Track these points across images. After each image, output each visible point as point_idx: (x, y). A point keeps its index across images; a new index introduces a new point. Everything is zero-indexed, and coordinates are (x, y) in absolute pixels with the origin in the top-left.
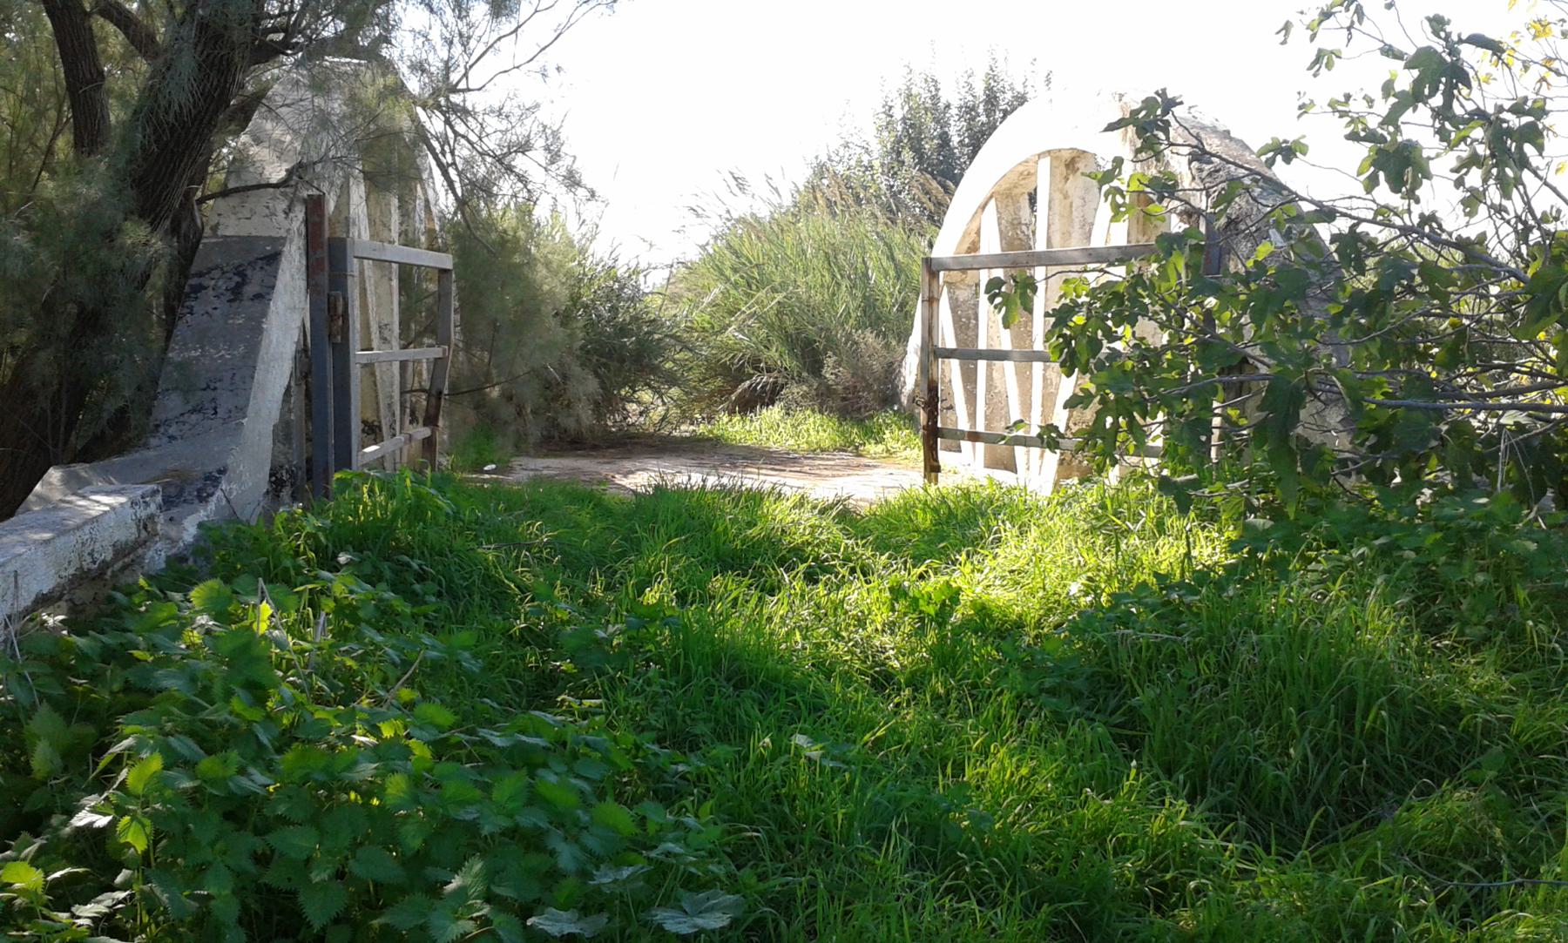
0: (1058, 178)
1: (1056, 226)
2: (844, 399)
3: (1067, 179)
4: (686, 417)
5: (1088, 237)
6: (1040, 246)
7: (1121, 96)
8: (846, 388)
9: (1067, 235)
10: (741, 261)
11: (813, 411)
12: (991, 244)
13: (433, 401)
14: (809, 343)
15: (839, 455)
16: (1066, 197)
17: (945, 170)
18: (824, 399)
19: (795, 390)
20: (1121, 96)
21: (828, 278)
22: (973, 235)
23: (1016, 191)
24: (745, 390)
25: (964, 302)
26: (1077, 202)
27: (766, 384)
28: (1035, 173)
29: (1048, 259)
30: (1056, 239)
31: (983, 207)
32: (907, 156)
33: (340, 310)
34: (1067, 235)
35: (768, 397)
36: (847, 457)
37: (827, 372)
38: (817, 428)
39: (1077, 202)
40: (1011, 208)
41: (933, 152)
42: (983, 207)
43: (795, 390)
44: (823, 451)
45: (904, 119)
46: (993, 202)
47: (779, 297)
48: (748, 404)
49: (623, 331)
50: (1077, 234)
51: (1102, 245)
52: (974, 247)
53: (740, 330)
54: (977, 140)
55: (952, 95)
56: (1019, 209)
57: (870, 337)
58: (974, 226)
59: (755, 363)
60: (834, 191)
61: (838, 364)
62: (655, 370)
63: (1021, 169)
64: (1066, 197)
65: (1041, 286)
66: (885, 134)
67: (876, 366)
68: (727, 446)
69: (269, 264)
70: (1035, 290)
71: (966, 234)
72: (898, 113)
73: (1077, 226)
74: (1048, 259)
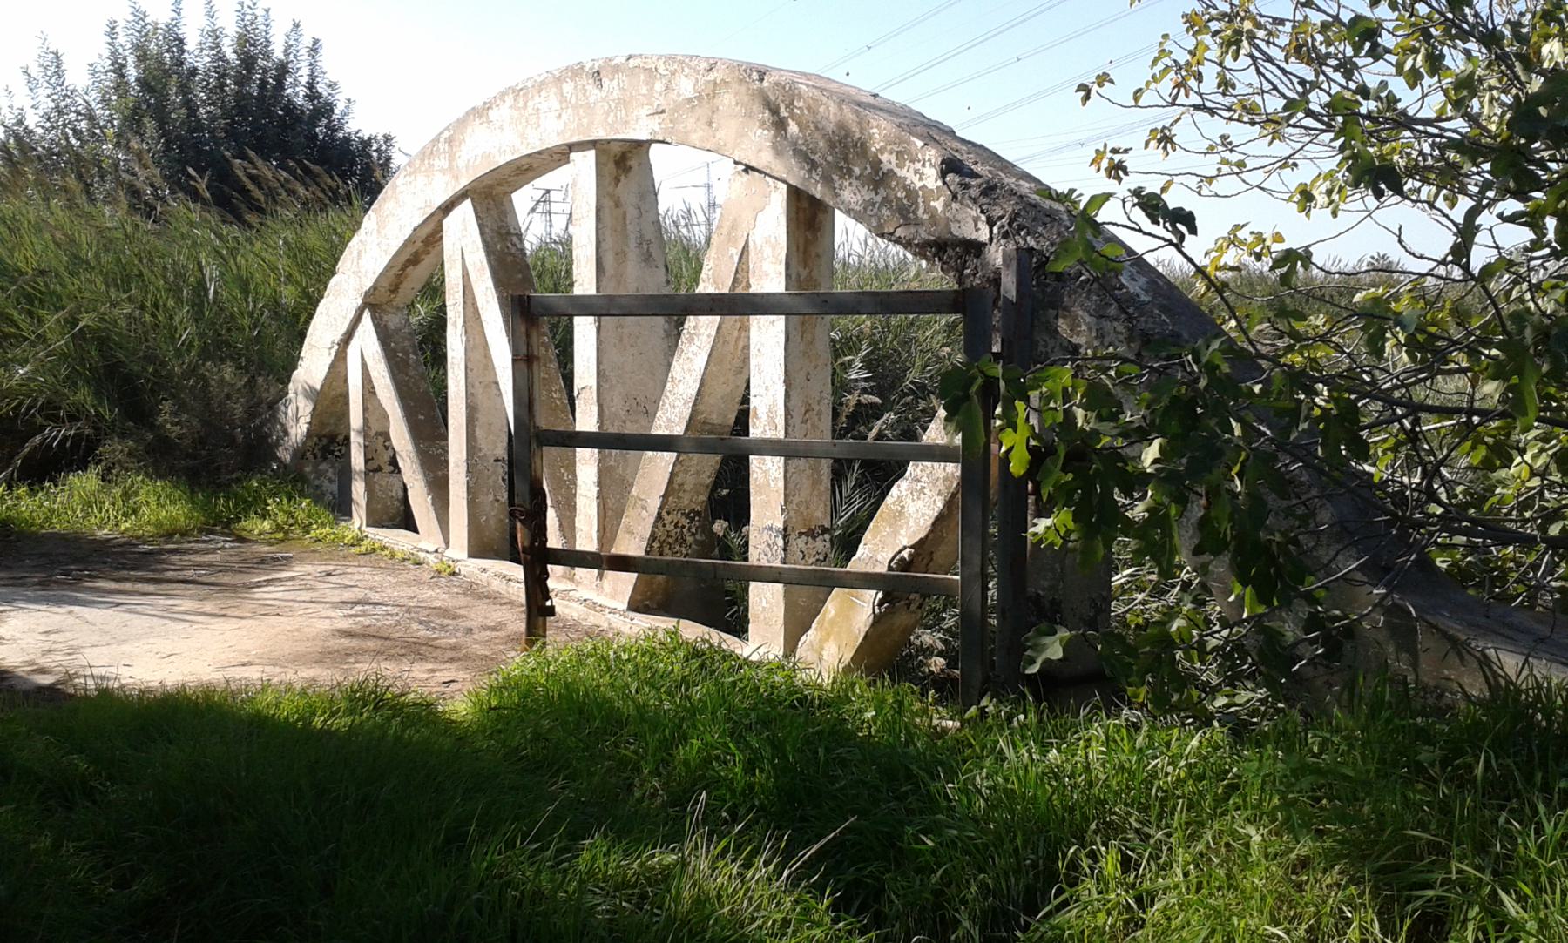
1: (608, 244)
3: (617, 181)
16: (617, 205)
18: (162, 459)
25: (398, 330)
26: (632, 212)
27: (65, 438)
31: (447, 208)
32: (150, 125)
35: (76, 456)
36: (220, 550)
38: (158, 506)
39: (632, 212)
43: (114, 448)
44: (184, 534)
45: (137, 80)
46: (467, 205)
48: (44, 470)
55: (197, 56)
59: (51, 412)
61: (182, 407)
62: (1493, 687)
64: (617, 205)
73: (632, 244)
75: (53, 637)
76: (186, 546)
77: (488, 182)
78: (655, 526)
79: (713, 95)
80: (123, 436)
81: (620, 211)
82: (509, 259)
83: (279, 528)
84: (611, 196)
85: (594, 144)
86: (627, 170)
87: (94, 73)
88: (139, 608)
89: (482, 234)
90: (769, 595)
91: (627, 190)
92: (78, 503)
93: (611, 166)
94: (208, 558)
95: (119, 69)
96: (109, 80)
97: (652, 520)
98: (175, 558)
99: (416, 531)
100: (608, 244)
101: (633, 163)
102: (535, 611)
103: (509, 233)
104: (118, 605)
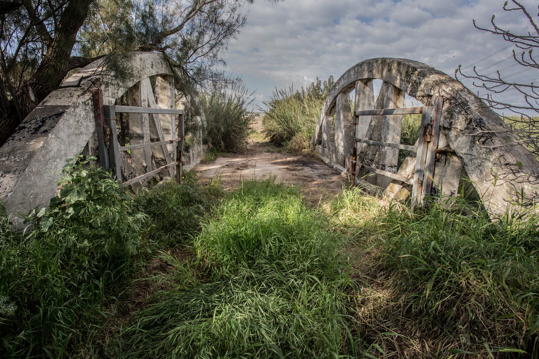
33: (108, 132)
88: (518, 44)
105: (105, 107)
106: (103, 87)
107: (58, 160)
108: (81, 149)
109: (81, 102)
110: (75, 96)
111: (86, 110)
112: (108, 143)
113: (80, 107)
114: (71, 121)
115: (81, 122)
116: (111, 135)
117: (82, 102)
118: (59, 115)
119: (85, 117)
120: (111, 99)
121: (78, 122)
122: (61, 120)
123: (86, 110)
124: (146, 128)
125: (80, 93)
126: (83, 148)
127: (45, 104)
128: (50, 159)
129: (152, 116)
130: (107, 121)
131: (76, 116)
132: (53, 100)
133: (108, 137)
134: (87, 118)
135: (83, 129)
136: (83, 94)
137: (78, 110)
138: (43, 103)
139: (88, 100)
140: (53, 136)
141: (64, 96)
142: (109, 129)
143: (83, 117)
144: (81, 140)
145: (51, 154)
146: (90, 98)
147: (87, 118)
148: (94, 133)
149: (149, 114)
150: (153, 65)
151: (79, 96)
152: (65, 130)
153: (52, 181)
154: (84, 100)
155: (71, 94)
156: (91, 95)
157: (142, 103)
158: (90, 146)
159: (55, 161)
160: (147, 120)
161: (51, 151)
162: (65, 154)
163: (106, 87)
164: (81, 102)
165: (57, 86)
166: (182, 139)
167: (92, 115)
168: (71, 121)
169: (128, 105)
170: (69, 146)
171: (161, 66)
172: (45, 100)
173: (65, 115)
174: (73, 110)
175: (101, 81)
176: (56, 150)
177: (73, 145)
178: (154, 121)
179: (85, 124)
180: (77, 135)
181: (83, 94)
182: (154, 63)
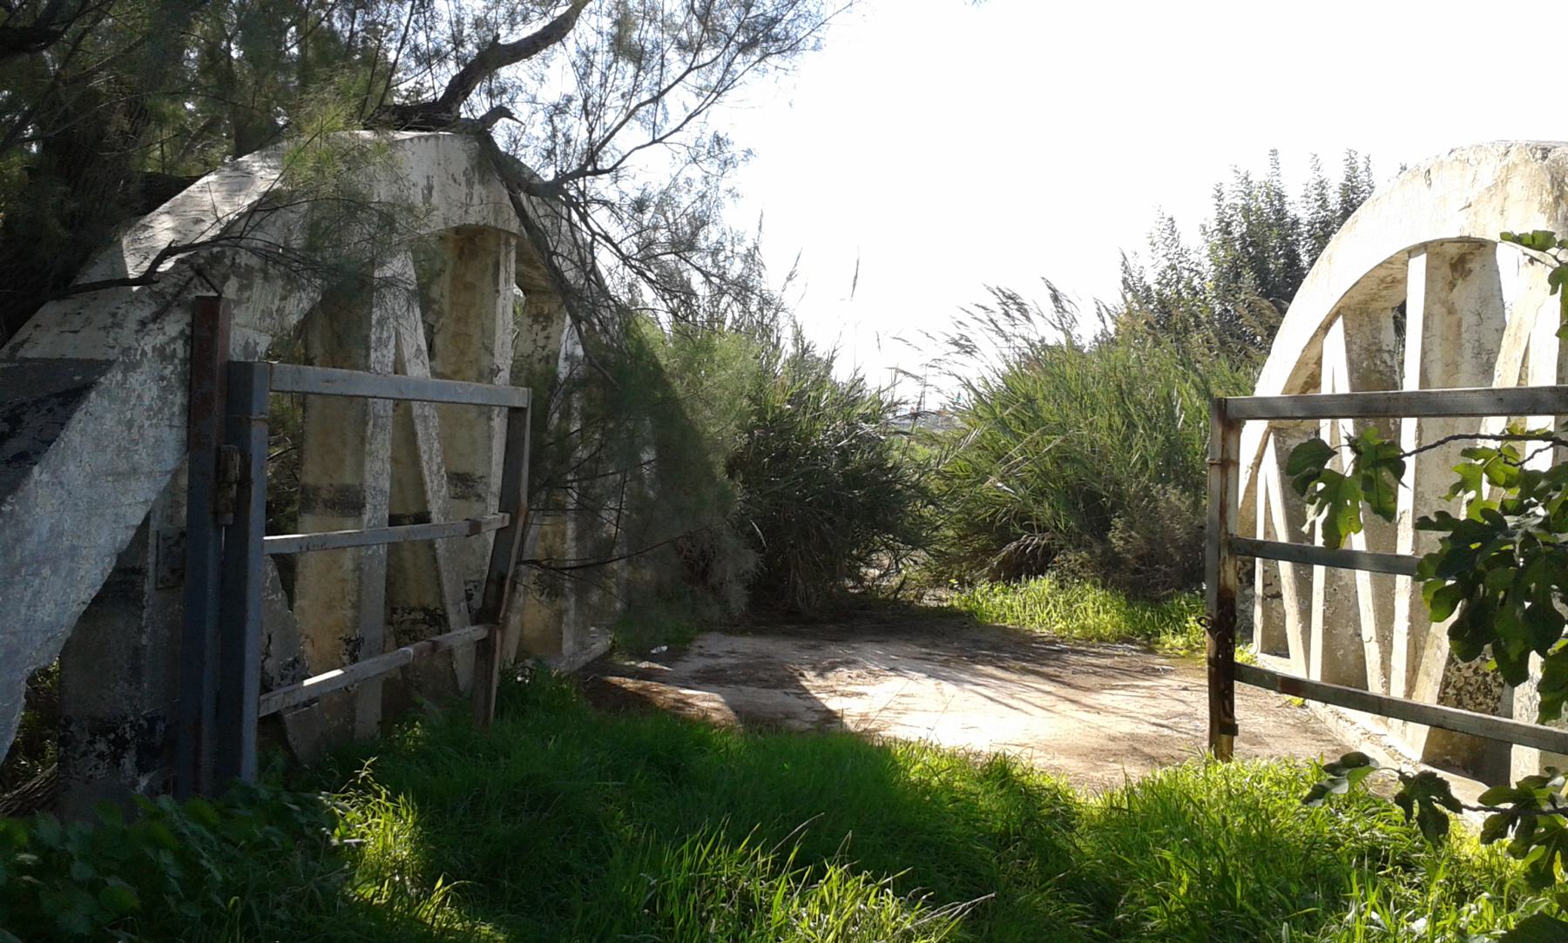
0: (1440, 285)
1: (1436, 354)
2: (1137, 571)
3: (1452, 285)
4: (938, 582)
5: (1488, 370)
6: (1411, 383)
7: (1546, 152)
8: (1140, 558)
9: (1452, 368)
10: (1037, 393)
11: (1095, 584)
12: (1336, 379)
13: (493, 588)
14: (1092, 497)
15: (1121, 649)
16: (1451, 312)
17: (1281, 285)
19: (1073, 558)
20: (1546, 152)
21: (1117, 420)
22: (1312, 366)
23: (1375, 305)
24: (1010, 553)
26: (1469, 319)
28: (1404, 280)
29: (1423, 406)
30: (1436, 372)
31: (1325, 327)
32: (1248, 277)
33: (235, 472)
34: (1452, 368)
36: (1128, 654)
37: (1116, 539)
38: (1096, 610)
39: (1469, 319)
40: (1367, 330)
41: (1267, 258)
42: (1325, 327)
44: (1101, 640)
47: (1058, 441)
48: (1018, 569)
49: (854, 479)
50: (1467, 366)
51: (1329, 392)
52: (1314, 381)
53: (1003, 479)
54: (1323, 233)
56: (1379, 330)
57: (1173, 494)
58: (1314, 353)
59: (1023, 518)
60: (1162, 317)
61: (1130, 526)
63: (1383, 273)
64: (1451, 312)
65: (1410, 462)
66: (1222, 253)
67: (1180, 532)
68: (978, 625)
69: (63, 405)
70: (1399, 470)
71: (1301, 364)
72: (1237, 231)
73: (1468, 352)
74: (1423, 406)
75: (904, 700)
76: (1101, 650)
77: (1358, 298)
78: (1447, 669)
79: (1505, 182)
80: (1078, 547)
81: (1454, 318)
82: (1375, 376)
83: (1189, 647)
84: (1444, 303)
85: (1424, 247)
86: (1466, 273)
87: (1205, 233)
88: (979, 689)
89: (1348, 351)
90: (1526, 759)
91: (1465, 296)
92: (1031, 604)
93: (1446, 270)
94: (1107, 662)
95: (1225, 229)
96: (1217, 238)
97: (1444, 662)
98: (1074, 658)
99: (1288, 656)
100: (1436, 354)
101: (1475, 265)
102: (1217, 728)
103: (1380, 350)
104: (1049, 693)
105: (231, 365)
106: (230, 290)
107: (46, 571)
108: (124, 537)
109: (148, 349)
110: (131, 325)
111: (163, 378)
112: (229, 518)
113: (146, 366)
114: (109, 421)
115: (141, 427)
116: (245, 483)
117: (154, 348)
118: (75, 395)
119: (156, 405)
120: (253, 336)
121: (130, 425)
122: (78, 415)
123: (163, 378)
124: (378, 466)
125: (147, 312)
126: (132, 533)
127: (21, 353)
128: (22, 564)
129: (409, 411)
130: (236, 430)
131: (125, 401)
132: (49, 337)
133: (233, 493)
134: (161, 410)
135: (142, 457)
136: (156, 317)
137: (135, 379)
138: (15, 349)
139: (174, 340)
140: (45, 477)
141: (88, 321)
142: (238, 458)
143: (150, 409)
144: (126, 500)
145: (31, 544)
146: (182, 332)
147: (161, 410)
148: (175, 474)
149: (398, 402)
150: (430, 188)
151: (143, 324)
152: (86, 458)
153: (18, 652)
154: (160, 340)
155: (114, 315)
156: (188, 318)
157: (373, 355)
158: (154, 525)
159: (35, 574)
160: (383, 429)
161: (30, 533)
162: (73, 548)
163: (242, 288)
164: (148, 349)
165: (64, 285)
166: (513, 520)
167: (179, 399)
168: (109, 421)
169: (309, 362)
170: (89, 519)
171: (464, 189)
172: (18, 338)
173: (93, 395)
174: (119, 377)
175: (227, 262)
176: (44, 528)
177: (102, 515)
178: (415, 434)
179: (150, 433)
180: (118, 475)
181: (156, 317)
182: (436, 182)
